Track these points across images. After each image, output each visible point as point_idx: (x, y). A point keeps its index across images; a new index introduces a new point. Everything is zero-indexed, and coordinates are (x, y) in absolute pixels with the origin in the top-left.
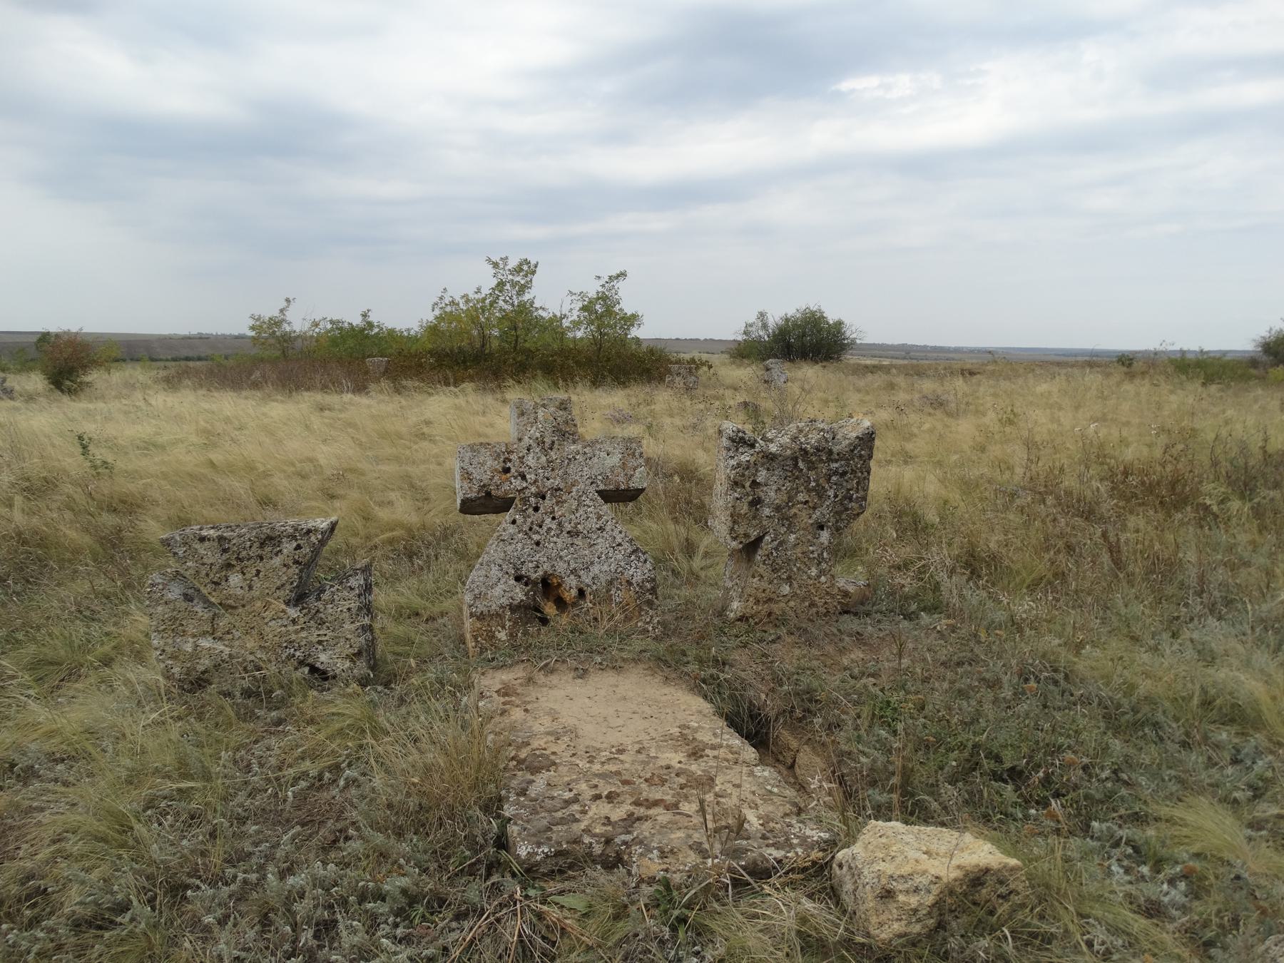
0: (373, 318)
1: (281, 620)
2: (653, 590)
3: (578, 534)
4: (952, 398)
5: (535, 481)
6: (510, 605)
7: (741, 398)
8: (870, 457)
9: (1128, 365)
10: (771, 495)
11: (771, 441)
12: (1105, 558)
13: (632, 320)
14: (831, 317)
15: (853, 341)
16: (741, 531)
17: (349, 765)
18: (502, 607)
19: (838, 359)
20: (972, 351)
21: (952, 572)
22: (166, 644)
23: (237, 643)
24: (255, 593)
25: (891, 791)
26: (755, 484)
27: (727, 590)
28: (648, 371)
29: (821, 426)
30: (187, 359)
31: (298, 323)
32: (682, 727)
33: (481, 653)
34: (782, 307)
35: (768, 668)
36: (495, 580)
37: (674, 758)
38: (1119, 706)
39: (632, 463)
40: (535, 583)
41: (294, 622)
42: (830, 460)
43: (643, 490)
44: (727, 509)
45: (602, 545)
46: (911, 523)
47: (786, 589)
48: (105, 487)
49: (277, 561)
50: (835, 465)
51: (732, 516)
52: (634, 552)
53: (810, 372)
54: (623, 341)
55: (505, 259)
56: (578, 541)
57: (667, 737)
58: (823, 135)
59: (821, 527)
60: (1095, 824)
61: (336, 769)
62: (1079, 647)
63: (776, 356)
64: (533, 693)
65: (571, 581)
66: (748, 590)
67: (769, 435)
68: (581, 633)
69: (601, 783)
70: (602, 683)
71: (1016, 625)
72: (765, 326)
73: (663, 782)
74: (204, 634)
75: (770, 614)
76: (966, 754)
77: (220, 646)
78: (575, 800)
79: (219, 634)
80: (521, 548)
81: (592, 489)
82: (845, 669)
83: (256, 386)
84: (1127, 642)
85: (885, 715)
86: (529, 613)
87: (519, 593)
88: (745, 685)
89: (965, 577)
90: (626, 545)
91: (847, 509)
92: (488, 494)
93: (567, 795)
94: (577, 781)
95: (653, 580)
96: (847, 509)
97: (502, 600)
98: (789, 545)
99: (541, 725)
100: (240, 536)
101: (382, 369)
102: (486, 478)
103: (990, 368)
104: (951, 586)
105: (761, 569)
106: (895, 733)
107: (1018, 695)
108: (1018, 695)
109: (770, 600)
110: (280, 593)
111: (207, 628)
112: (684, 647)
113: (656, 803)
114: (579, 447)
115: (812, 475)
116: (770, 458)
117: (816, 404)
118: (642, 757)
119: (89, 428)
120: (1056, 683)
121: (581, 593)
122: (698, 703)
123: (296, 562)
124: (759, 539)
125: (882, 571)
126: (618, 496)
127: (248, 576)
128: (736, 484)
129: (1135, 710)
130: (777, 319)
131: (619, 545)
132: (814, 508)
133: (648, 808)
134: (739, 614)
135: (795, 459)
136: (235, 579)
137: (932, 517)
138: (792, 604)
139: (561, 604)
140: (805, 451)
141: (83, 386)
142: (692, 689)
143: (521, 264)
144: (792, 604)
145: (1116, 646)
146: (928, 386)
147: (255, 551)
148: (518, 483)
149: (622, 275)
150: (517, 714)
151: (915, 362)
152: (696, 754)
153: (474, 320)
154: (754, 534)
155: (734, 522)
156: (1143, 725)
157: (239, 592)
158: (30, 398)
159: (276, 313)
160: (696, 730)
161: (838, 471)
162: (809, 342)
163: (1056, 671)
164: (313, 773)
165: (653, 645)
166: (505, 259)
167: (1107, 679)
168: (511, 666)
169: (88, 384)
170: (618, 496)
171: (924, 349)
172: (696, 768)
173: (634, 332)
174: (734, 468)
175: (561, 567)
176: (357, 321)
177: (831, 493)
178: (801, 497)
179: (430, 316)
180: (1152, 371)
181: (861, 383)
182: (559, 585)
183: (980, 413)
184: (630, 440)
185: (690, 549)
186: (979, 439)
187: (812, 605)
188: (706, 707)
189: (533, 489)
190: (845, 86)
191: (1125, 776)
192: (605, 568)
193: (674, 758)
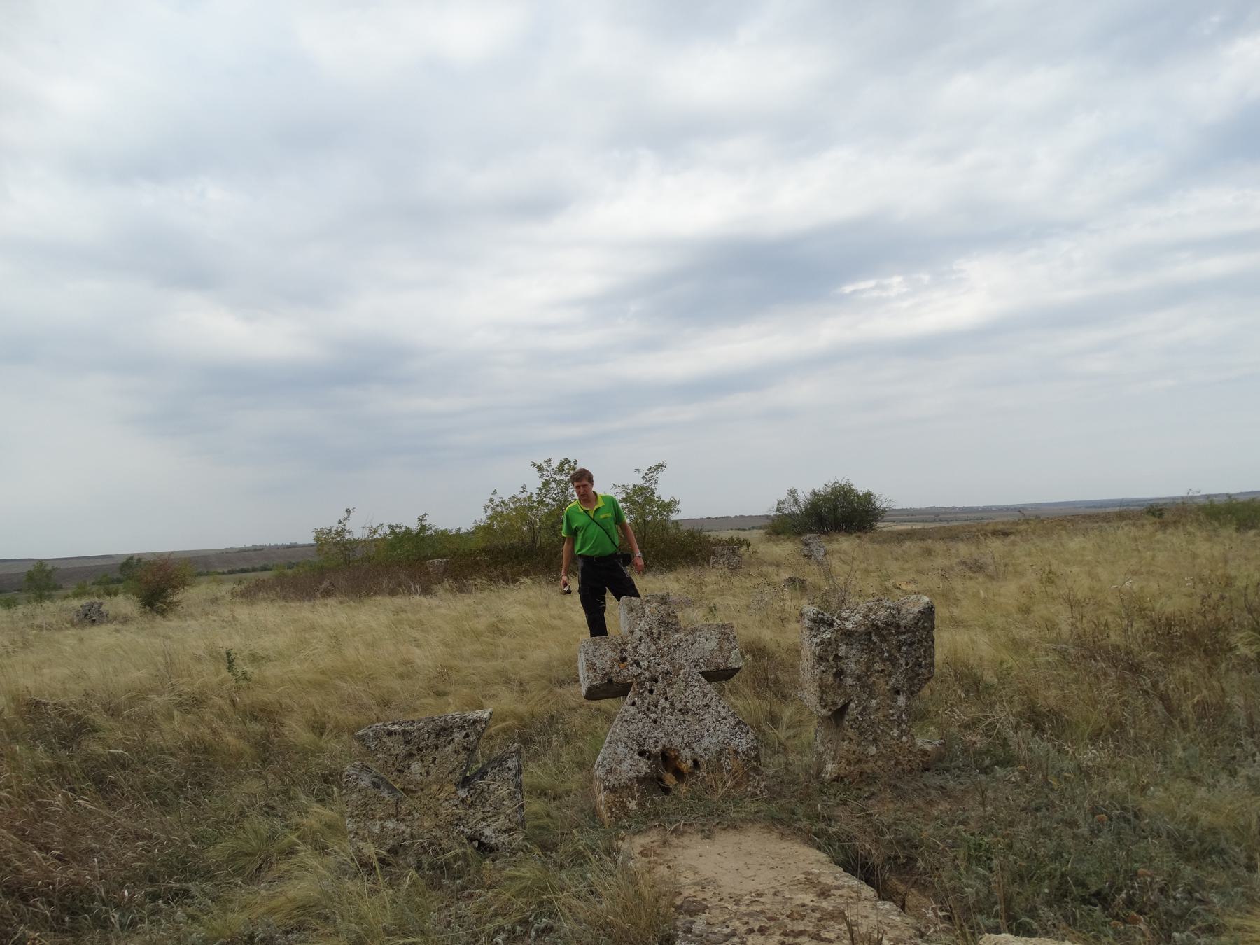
0: (427, 523)
1: (450, 802)
2: (757, 758)
3: (688, 711)
4: (990, 561)
5: (649, 667)
6: (637, 777)
7: (785, 575)
8: (933, 628)
9: (1160, 514)
10: (852, 666)
11: (846, 619)
12: (1159, 706)
13: (669, 506)
14: (861, 488)
15: (884, 511)
16: (829, 700)
17: (536, 918)
18: (630, 780)
19: (872, 529)
20: (1001, 509)
21: (1017, 727)
22: (359, 827)
23: (416, 823)
24: (432, 778)
25: (996, 916)
26: (837, 658)
27: (820, 754)
28: (692, 553)
29: (887, 604)
30: (243, 571)
31: (357, 530)
32: (806, 873)
33: (617, 822)
34: (811, 482)
35: (868, 822)
36: (621, 756)
37: (808, 898)
38: (1186, 837)
39: (727, 646)
40: (656, 757)
41: (463, 801)
42: (898, 633)
43: (739, 669)
44: (814, 681)
45: (709, 719)
46: (974, 686)
47: (873, 750)
48: (245, 699)
49: (450, 748)
50: (903, 637)
51: (820, 686)
52: (737, 724)
53: (845, 544)
54: (663, 525)
55: (548, 462)
56: (689, 718)
57: (796, 883)
58: (828, 330)
59: (898, 693)
60: (1176, 935)
61: (525, 922)
62: (1144, 788)
63: (811, 531)
64: (670, 853)
65: (687, 754)
66: (840, 753)
67: (844, 615)
68: (700, 800)
69: (751, 920)
70: (726, 841)
71: (1084, 773)
72: (796, 502)
73: (803, 917)
74: (390, 816)
75: (861, 774)
76: (1056, 882)
77: (402, 827)
78: (733, 934)
79: (402, 816)
80: (641, 726)
81: (696, 671)
82: (936, 819)
83: (328, 593)
84: (1189, 783)
85: (979, 855)
86: (653, 784)
87: (644, 767)
88: (851, 838)
89: (1030, 732)
90: (730, 719)
91: (918, 675)
92: (610, 681)
93: (726, 931)
94: (730, 919)
95: (756, 748)
96: (918, 675)
97: (630, 774)
98: (872, 710)
99: (687, 878)
100: (419, 729)
101: (441, 570)
102: (607, 667)
103: (1022, 527)
104: (1019, 740)
105: (850, 733)
106: (991, 870)
107: (1095, 832)
108: (1095, 832)
109: (860, 761)
110: (451, 777)
111: (392, 811)
112: (792, 808)
113: (802, 933)
114: (682, 635)
115: (885, 646)
116: (848, 634)
117: (865, 580)
118: (779, 898)
119: (235, 642)
120: (1128, 821)
121: (696, 764)
122: (815, 854)
123: (465, 749)
124: (845, 706)
125: (954, 730)
126: (718, 676)
127: (426, 763)
128: (821, 659)
129: (1201, 840)
130: (808, 495)
131: (724, 718)
132: (890, 676)
133: (796, 937)
134: (834, 775)
135: (869, 634)
136: (416, 767)
137: (990, 678)
138: (880, 763)
139: (679, 775)
140: (877, 626)
141: (173, 606)
142: (805, 843)
143: (562, 465)
144: (880, 763)
145: (1180, 786)
146: (964, 550)
147: (432, 741)
148: (634, 670)
149: (661, 467)
150: (662, 871)
151: (945, 524)
152: (824, 893)
153: (524, 518)
154: (841, 702)
155: (823, 692)
156: (1210, 853)
157: (419, 778)
158: (125, 620)
159: (335, 525)
160: (819, 875)
161: (904, 643)
162: (840, 515)
163: (1124, 808)
164: (508, 927)
165: (764, 807)
166: (548, 462)
167: (1173, 814)
168: (646, 831)
169: (178, 603)
170: (718, 676)
171: (953, 510)
172: (826, 904)
173: (674, 517)
174: (817, 645)
175: (677, 742)
176: (414, 525)
177: (903, 661)
178: (877, 667)
179: (482, 517)
180: (1183, 520)
181: (898, 550)
182: (677, 757)
183: (1019, 574)
184: (724, 626)
185: (774, 720)
186: (1022, 601)
187: (898, 763)
188: (822, 856)
189: (647, 674)
190: (848, 289)
191: (1198, 895)
192: (714, 740)
193: (808, 898)
